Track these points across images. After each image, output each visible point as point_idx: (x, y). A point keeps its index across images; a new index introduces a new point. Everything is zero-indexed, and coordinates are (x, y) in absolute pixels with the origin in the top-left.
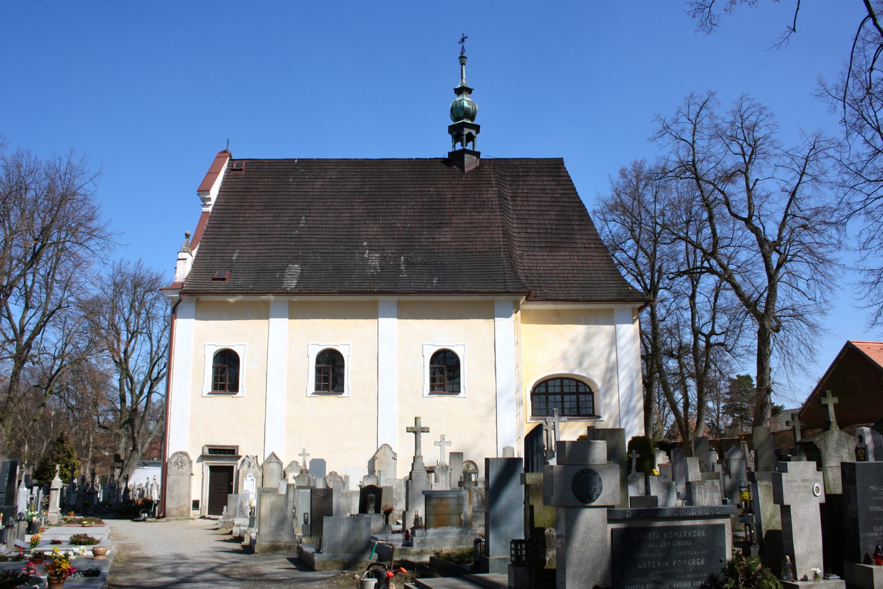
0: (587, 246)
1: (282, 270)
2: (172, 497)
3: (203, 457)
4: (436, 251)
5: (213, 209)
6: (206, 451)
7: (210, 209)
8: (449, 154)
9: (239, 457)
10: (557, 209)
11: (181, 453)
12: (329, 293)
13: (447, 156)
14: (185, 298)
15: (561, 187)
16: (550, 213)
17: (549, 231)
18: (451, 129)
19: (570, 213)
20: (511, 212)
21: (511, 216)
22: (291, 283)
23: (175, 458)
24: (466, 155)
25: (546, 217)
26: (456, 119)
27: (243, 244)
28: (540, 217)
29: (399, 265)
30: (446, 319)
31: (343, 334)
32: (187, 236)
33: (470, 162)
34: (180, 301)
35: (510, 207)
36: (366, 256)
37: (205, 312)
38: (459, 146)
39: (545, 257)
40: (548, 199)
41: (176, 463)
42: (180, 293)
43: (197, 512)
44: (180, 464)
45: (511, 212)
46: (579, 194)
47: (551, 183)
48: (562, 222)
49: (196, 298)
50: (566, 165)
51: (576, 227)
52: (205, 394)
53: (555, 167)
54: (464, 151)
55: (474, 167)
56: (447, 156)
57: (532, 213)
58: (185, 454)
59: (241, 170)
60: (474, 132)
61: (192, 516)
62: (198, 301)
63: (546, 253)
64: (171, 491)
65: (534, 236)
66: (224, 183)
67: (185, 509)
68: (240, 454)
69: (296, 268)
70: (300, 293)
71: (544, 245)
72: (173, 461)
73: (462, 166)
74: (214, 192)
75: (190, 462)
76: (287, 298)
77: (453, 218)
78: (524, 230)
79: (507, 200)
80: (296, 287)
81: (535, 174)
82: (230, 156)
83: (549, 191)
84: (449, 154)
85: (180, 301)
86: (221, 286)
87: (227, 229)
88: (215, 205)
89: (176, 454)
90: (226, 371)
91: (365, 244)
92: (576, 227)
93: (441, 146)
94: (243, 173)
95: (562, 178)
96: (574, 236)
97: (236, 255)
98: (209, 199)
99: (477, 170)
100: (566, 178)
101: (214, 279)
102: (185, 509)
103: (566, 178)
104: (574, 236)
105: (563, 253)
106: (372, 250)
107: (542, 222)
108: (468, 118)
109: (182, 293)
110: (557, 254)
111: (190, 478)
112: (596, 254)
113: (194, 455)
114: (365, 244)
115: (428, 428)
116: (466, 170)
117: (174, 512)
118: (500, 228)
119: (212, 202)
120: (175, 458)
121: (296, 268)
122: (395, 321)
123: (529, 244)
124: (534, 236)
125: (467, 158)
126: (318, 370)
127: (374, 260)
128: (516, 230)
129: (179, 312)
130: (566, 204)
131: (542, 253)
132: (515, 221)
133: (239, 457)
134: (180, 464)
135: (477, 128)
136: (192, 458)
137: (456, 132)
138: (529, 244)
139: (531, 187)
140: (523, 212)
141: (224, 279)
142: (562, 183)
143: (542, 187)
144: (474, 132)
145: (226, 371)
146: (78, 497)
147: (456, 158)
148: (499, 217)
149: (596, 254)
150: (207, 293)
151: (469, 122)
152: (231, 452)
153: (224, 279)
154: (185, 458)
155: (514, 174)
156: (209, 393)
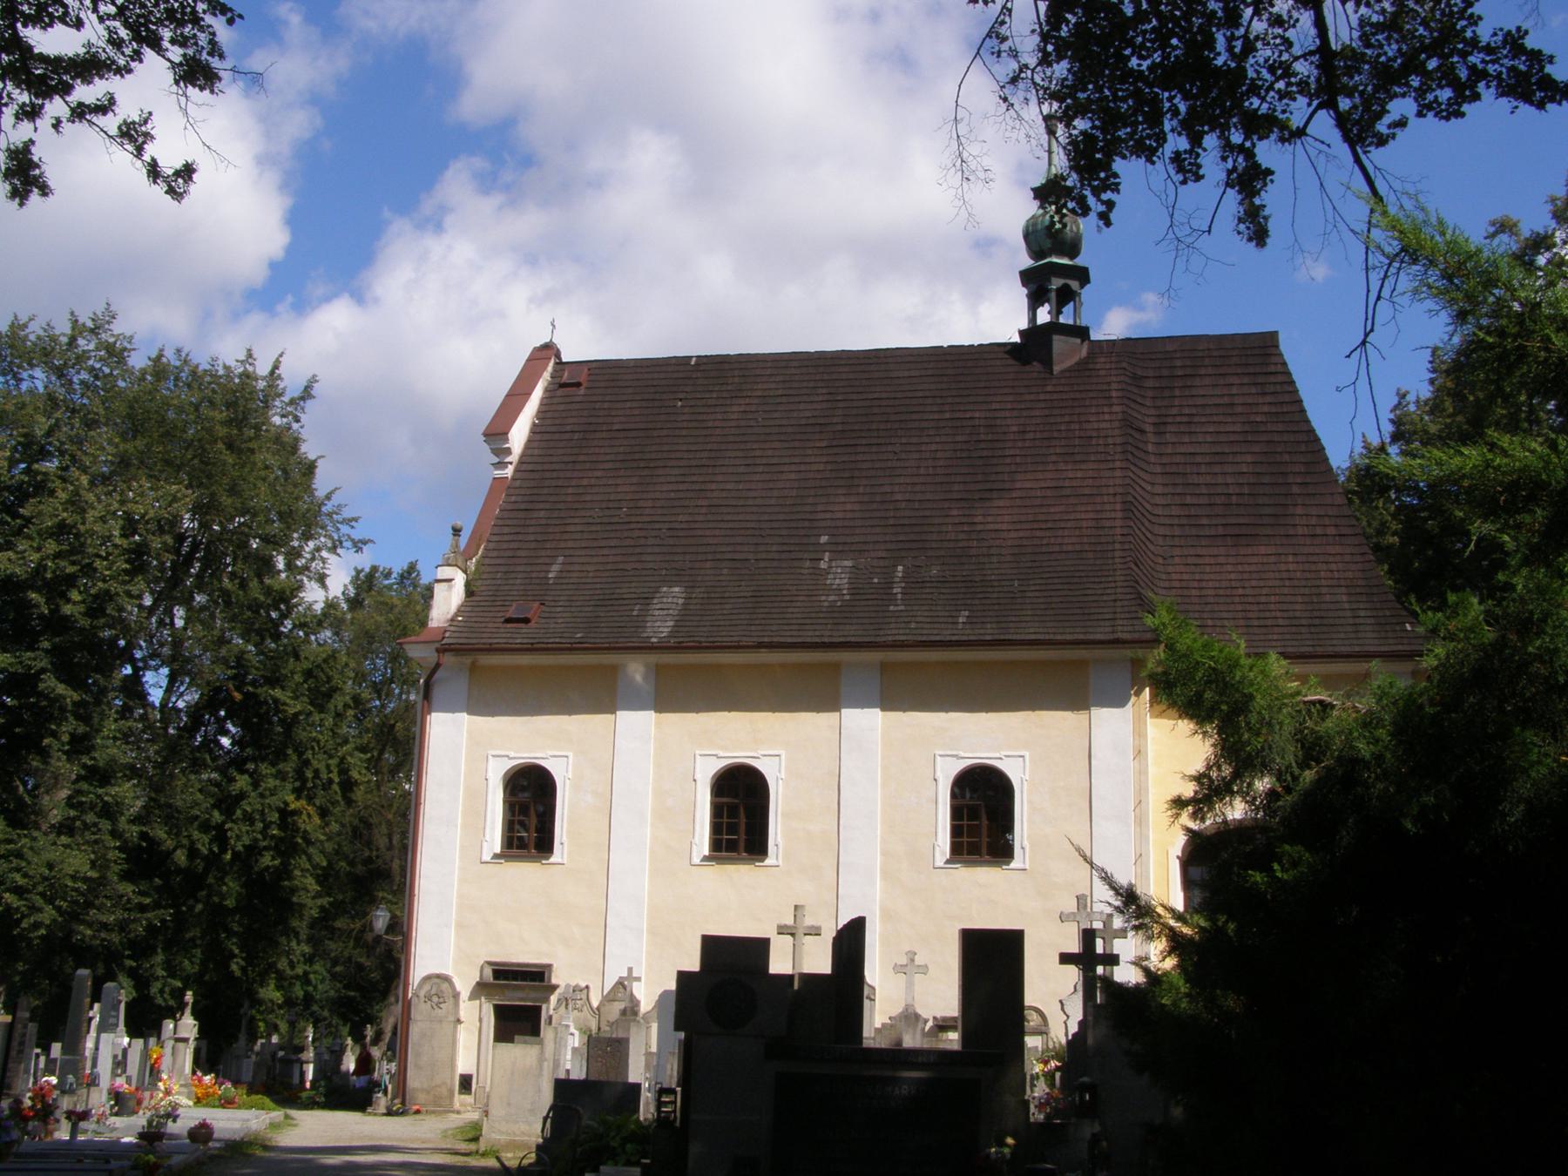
0: (1319, 531)
1: (646, 600)
2: (418, 1067)
3: (481, 989)
4: (973, 552)
5: (516, 471)
6: (488, 972)
7: (509, 471)
8: (1022, 333)
9: (555, 987)
10: (1257, 449)
11: (438, 976)
12: (737, 647)
13: (1016, 339)
14: (448, 659)
15: (1269, 399)
16: (1239, 459)
17: (1234, 499)
18: (1027, 277)
19: (1287, 458)
20: (1152, 459)
21: (1151, 468)
22: (660, 627)
23: (427, 987)
24: (1056, 338)
25: (1229, 469)
26: (1036, 252)
27: (570, 544)
28: (1217, 469)
29: (889, 584)
30: (774, 710)
31: (552, 740)
32: (457, 531)
33: (1064, 352)
34: (438, 666)
35: (1150, 448)
36: (823, 565)
37: (493, 694)
38: (1043, 315)
39: (1222, 560)
40: (1238, 428)
41: (429, 998)
42: (438, 650)
43: (469, 1099)
44: (435, 999)
45: (1152, 459)
46: (1311, 415)
47: (1245, 390)
48: (1266, 479)
49: (468, 660)
50: (1283, 348)
51: (1295, 490)
52: (487, 857)
53: (1259, 352)
54: (1054, 327)
55: (1075, 360)
56: (1016, 339)
57: (1199, 459)
58: (446, 979)
59: (578, 385)
60: (1074, 285)
61: (457, 1105)
62: (473, 668)
63: (1222, 551)
64: (418, 1055)
65: (1199, 512)
66: (542, 413)
67: (444, 1092)
68: (554, 981)
69: (674, 595)
70: (679, 648)
71: (1221, 531)
72: (422, 993)
73: (1047, 362)
74: (519, 435)
75: (456, 996)
76: (653, 658)
77: (1019, 477)
78: (1178, 500)
79: (1142, 432)
80: (672, 635)
81: (1210, 371)
82: (558, 355)
83: (1239, 409)
84: (1022, 333)
85: (438, 666)
86: (522, 634)
87: (542, 514)
88: (521, 462)
89: (428, 978)
90: (531, 808)
91: (824, 539)
92: (1295, 490)
93: (999, 316)
94: (582, 391)
95: (1272, 379)
96: (1291, 510)
97: (556, 568)
98: (508, 451)
99: (1083, 367)
100: (1280, 378)
101: (509, 621)
102: (444, 1092)
103: (1280, 378)
104: (1291, 510)
105: (1263, 550)
106: (839, 551)
107: (1220, 480)
108: (1061, 254)
109: (442, 650)
110: (1249, 550)
111: (455, 1028)
112: (1338, 549)
113: (464, 986)
114: (824, 539)
115: (819, 928)
116: (1057, 369)
117: (422, 1098)
118: (1119, 498)
119: (514, 457)
120: (427, 987)
121: (674, 595)
122: (650, 715)
123: (1188, 531)
124: (1199, 512)
125: (1059, 343)
126: (957, 813)
127: (839, 574)
128: (1158, 500)
129: (438, 693)
130: (1276, 438)
131: (1215, 551)
132: (1159, 479)
133: (555, 987)
134: (435, 999)
135: (1083, 275)
136: (459, 987)
137: (1037, 284)
138: (1188, 531)
139: (1200, 401)
140: (1178, 459)
141: (526, 621)
142: (1271, 389)
143: (1226, 400)
144: (1074, 285)
145: (531, 808)
146: (258, 1065)
147: (1035, 341)
148: (1118, 473)
149: (1338, 549)
150: (491, 650)
151: (1065, 261)
152: (536, 976)
153: (526, 621)
154: (445, 986)
155: (1165, 372)
156: (496, 856)
